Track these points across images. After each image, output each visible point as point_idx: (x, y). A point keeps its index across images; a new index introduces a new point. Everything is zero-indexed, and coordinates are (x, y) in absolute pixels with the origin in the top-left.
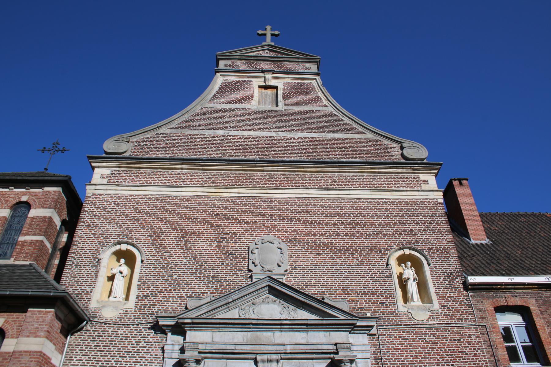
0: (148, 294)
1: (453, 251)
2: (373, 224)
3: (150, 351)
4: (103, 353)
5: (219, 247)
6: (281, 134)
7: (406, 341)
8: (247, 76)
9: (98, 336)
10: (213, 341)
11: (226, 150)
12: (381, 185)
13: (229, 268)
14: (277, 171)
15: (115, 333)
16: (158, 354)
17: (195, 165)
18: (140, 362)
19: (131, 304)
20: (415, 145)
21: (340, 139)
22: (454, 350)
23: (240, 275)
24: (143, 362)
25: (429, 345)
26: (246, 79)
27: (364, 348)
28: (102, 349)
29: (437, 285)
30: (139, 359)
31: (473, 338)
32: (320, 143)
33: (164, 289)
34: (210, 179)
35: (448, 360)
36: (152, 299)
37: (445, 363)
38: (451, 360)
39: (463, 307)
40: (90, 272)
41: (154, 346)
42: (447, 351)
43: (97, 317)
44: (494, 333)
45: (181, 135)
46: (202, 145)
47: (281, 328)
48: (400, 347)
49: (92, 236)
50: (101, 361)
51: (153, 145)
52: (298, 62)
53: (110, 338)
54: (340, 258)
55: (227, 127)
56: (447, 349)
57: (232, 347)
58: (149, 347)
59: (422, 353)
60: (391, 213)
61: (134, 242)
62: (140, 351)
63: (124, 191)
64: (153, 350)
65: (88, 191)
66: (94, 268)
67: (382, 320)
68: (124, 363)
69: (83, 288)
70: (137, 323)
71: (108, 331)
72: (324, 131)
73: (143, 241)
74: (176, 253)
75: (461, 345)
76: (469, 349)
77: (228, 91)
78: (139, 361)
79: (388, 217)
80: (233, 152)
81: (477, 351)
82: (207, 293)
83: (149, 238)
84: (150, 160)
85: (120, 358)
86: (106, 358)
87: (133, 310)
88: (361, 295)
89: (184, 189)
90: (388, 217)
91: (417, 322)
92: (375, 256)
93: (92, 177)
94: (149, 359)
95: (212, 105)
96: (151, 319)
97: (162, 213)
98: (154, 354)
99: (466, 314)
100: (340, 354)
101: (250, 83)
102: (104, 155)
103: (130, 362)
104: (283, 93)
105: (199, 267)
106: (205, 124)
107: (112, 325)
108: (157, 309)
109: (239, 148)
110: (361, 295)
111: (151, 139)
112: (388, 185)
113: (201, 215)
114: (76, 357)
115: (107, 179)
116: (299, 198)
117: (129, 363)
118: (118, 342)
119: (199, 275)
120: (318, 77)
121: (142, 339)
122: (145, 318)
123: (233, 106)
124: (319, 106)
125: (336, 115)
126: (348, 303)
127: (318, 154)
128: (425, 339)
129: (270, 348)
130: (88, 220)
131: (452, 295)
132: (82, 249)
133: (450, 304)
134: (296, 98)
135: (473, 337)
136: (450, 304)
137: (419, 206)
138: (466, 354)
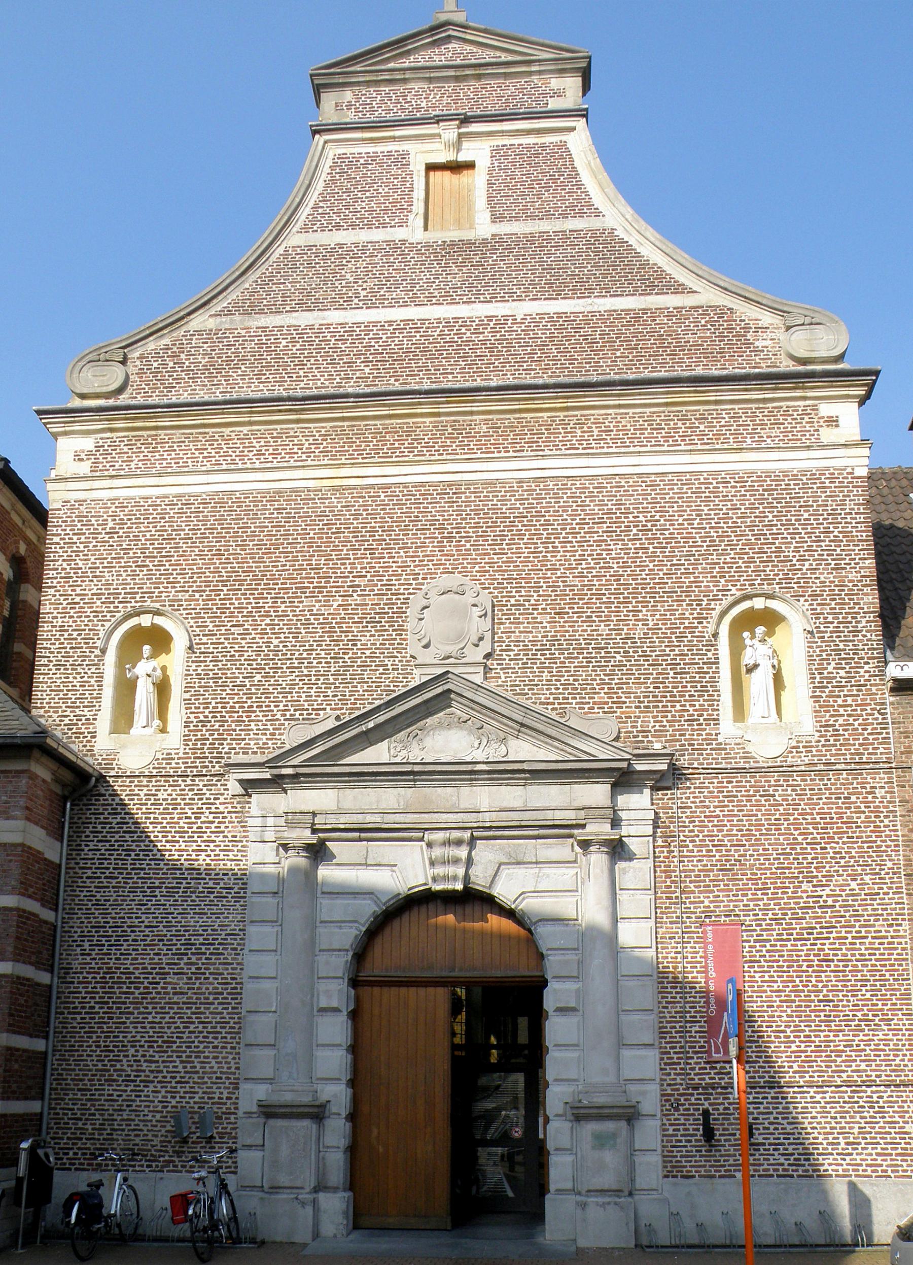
0: (206, 717)
3: (222, 829)
8: (394, 138)
10: (339, 808)
14: (472, 413)
15: (152, 798)
19: (174, 739)
21: (627, 311)
22: (832, 818)
23: (390, 667)
25: (781, 808)
31: (878, 795)
32: (577, 329)
33: (237, 705)
36: (216, 727)
37: (808, 844)
38: (822, 838)
39: (870, 727)
40: (86, 679)
41: (229, 819)
42: (818, 820)
43: (114, 769)
45: (243, 332)
47: (471, 780)
48: (718, 812)
49: (77, 599)
50: (134, 851)
52: (531, 73)
53: (144, 807)
56: (818, 817)
57: (377, 818)
66: (93, 669)
67: (686, 757)
68: (176, 853)
71: (138, 795)
73: (184, 603)
74: (255, 626)
75: (850, 808)
76: (866, 817)
77: (348, 191)
78: (203, 848)
79: (726, 517)
80: (367, 370)
81: (882, 821)
83: (197, 595)
85: (168, 845)
87: (182, 751)
90: (726, 517)
92: (687, 615)
94: (222, 844)
96: (217, 768)
98: (229, 835)
100: (589, 828)
101: (402, 160)
102: (77, 403)
105: (305, 655)
106: (297, 296)
112: (736, 434)
114: (87, 845)
115: (89, 463)
117: (185, 853)
118: (159, 814)
119: (306, 672)
120: (581, 123)
122: (207, 767)
123: (363, 236)
124: (581, 215)
130: (65, 565)
131: (849, 702)
132: (62, 629)
135: (879, 793)
137: (806, 487)
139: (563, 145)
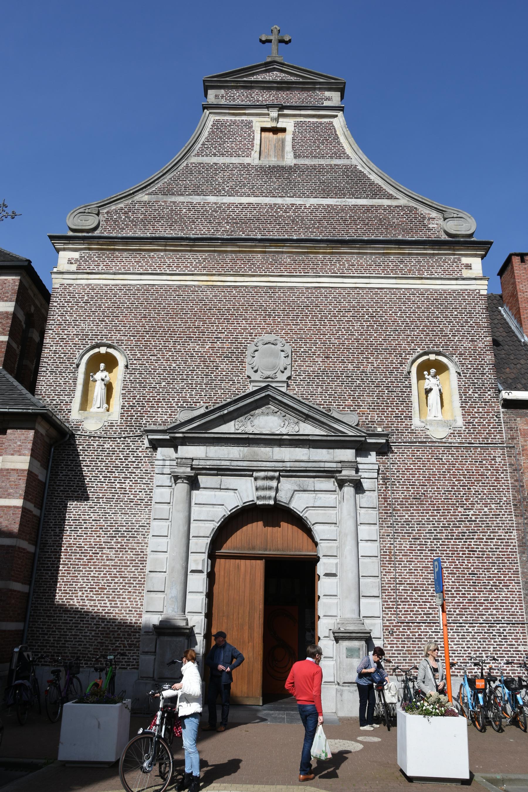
0: (134, 404)
1: (489, 357)
2: (395, 321)
3: (140, 466)
4: (90, 468)
5: (212, 348)
6: (289, 201)
7: (420, 461)
9: (83, 450)
10: (206, 457)
11: (219, 223)
12: (410, 271)
13: (224, 373)
15: (101, 447)
16: (149, 469)
17: (182, 245)
18: (130, 478)
20: (461, 215)
21: (363, 206)
22: (473, 472)
24: (133, 478)
25: (446, 466)
26: (244, 118)
27: (371, 467)
28: (89, 464)
29: (464, 398)
30: (128, 474)
32: (337, 214)
34: (200, 263)
35: (465, 483)
36: (139, 409)
39: (492, 425)
42: (466, 473)
43: (80, 430)
44: (523, 456)
45: (163, 204)
46: (189, 218)
48: (412, 467)
49: (65, 337)
51: (129, 217)
53: (96, 452)
54: (352, 362)
55: (220, 191)
56: (466, 472)
57: (228, 463)
58: (138, 462)
59: (437, 475)
60: (418, 307)
61: (115, 344)
62: (129, 466)
63: (96, 281)
64: (142, 465)
65: (54, 281)
66: (72, 375)
67: (395, 436)
68: (113, 479)
69: (61, 398)
70: (124, 436)
71: (93, 445)
72: (344, 196)
74: (163, 356)
76: (491, 473)
77: (220, 138)
78: (128, 476)
79: (414, 312)
80: (228, 227)
82: (200, 402)
83: (132, 338)
84: (127, 240)
85: (108, 474)
86: (94, 473)
87: (119, 422)
88: (374, 407)
89: (169, 277)
91: (434, 440)
92: (394, 361)
93: (57, 263)
94: (139, 474)
95: (200, 159)
96: (139, 432)
97: (146, 308)
98: (144, 469)
99: (494, 433)
101: (249, 125)
102: (71, 234)
103: (119, 477)
104: (293, 139)
105: (190, 373)
107: (97, 438)
108: (145, 421)
109: (236, 222)
110: (374, 407)
111: (126, 210)
112: (419, 270)
113: (192, 309)
115: (76, 265)
116: (307, 288)
118: (105, 456)
119: (190, 382)
121: (130, 453)
122: (133, 431)
124: (340, 157)
125: (361, 172)
126: (357, 416)
127: (335, 228)
128: (442, 459)
129: (268, 464)
132: (55, 352)
133: (476, 420)
134: (310, 146)
135: (498, 460)
136: (476, 420)
138: (487, 478)
139: (332, 123)
